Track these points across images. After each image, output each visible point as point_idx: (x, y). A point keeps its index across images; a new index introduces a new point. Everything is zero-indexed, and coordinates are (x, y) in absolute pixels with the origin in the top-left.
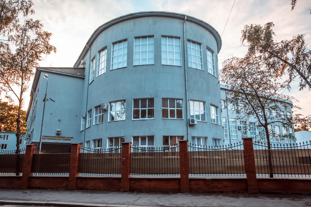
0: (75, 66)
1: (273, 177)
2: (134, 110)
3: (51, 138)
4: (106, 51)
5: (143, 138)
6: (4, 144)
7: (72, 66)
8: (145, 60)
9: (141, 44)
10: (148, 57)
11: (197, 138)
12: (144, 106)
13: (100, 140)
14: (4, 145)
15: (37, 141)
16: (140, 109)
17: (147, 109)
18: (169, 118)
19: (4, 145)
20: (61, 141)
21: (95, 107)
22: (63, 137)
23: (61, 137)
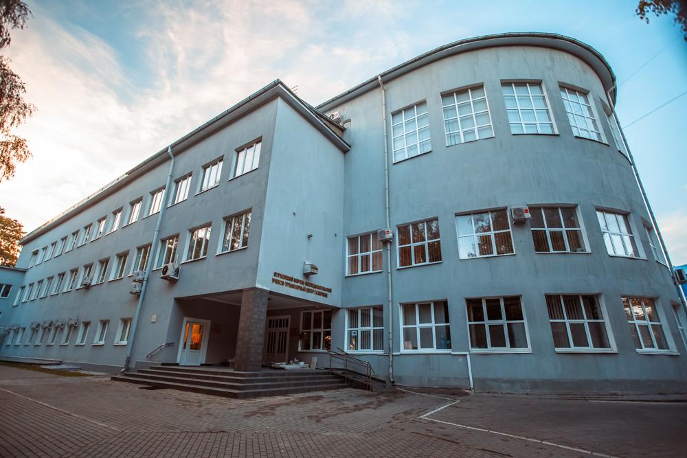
0: (320, 107)
1: (399, 351)
2: (509, 228)
3: (293, 283)
4: (258, 147)
5: (424, 307)
6: (497, 301)
7: (314, 105)
8: (472, 133)
9: (416, 117)
10: (418, 142)
11: (420, 306)
12: (554, 223)
13: (429, 305)
14: (4, 286)
15: (265, 288)
16: (412, 245)
17: (426, 243)
18: (414, 264)
19: (4, 286)
20: (312, 297)
21: (117, 255)
22: (316, 287)
23: (311, 285)
